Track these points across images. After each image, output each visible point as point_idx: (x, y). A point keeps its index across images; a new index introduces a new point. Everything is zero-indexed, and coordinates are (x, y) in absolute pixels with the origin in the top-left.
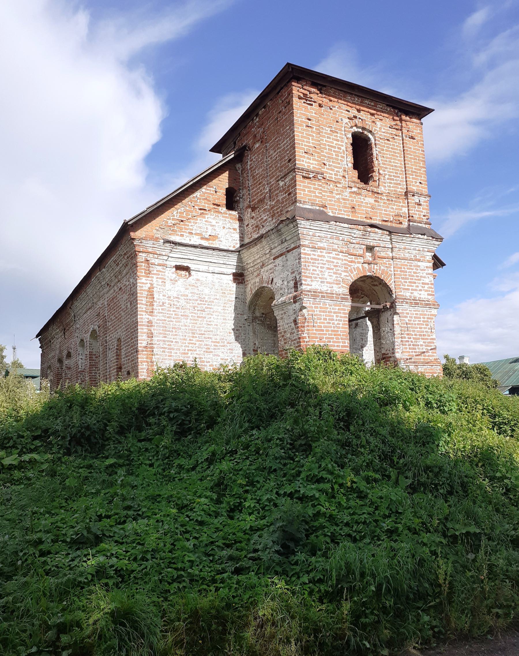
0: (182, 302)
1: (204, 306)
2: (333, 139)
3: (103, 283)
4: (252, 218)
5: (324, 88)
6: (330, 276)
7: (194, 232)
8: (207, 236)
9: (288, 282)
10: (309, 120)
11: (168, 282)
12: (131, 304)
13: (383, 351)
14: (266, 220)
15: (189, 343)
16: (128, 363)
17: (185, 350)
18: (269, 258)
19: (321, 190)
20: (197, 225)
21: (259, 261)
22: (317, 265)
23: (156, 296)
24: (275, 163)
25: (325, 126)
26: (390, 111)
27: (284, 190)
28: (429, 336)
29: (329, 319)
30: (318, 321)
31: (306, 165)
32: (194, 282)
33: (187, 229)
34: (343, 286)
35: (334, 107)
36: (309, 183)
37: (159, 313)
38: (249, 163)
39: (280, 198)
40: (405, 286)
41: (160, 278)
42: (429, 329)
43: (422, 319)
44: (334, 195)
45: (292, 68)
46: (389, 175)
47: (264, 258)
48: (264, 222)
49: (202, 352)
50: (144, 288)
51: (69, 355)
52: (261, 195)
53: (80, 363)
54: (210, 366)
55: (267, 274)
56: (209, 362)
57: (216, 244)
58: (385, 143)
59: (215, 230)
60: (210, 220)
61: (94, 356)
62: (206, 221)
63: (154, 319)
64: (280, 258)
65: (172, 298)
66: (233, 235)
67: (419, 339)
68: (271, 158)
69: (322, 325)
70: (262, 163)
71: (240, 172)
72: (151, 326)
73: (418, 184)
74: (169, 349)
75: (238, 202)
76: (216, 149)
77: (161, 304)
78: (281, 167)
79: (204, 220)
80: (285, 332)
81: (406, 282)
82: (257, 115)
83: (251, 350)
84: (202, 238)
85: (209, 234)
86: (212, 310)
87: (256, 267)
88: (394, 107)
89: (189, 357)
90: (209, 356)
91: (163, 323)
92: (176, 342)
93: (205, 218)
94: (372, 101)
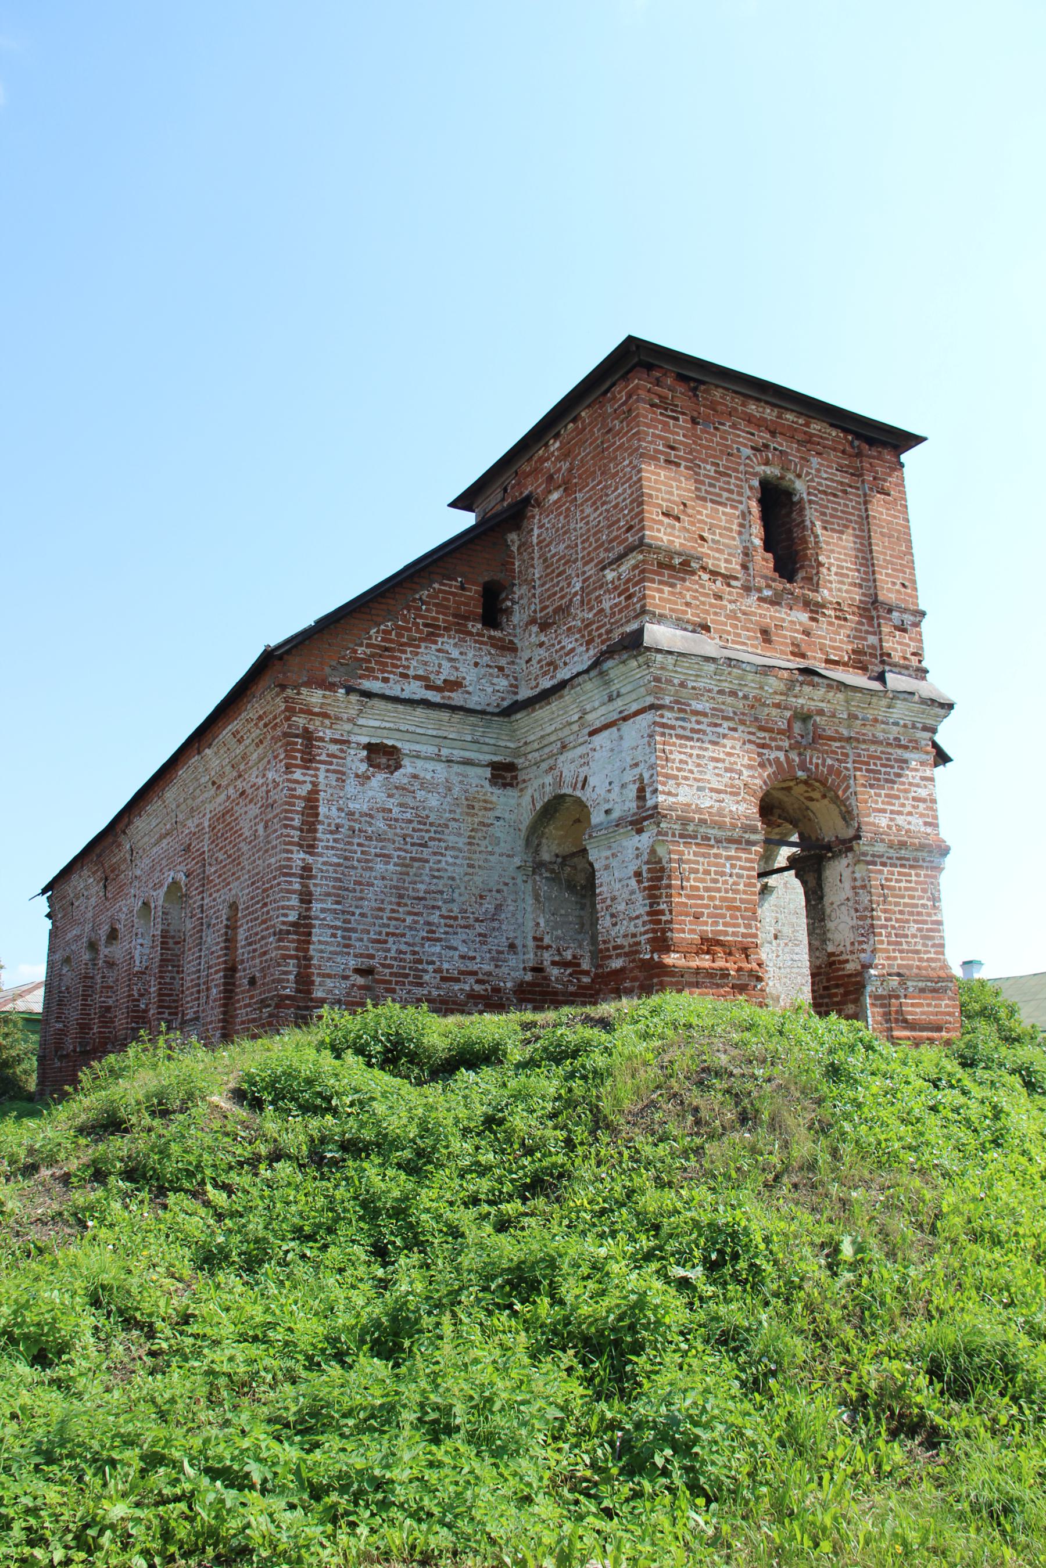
0: (380, 824)
1: (427, 836)
2: (721, 488)
3: (203, 780)
4: (541, 645)
5: (702, 387)
6: (718, 775)
7: (411, 672)
8: (439, 683)
9: (623, 786)
10: (673, 448)
11: (351, 782)
12: (266, 827)
13: (830, 948)
14: (573, 650)
15: (390, 919)
16: (253, 958)
17: (380, 933)
18: (577, 733)
19: (697, 591)
20: (419, 657)
21: (553, 738)
22: (688, 750)
23: (322, 810)
24: (595, 534)
25: (705, 462)
26: (837, 436)
27: (616, 588)
28: (929, 915)
29: (716, 873)
30: (692, 876)
31: (665, 538)
32: (405, 781)
33: (398, 667)
34: (744, 800)
35: (723, 424)
36: (670, 576)
37: (327, 848)
38: (536, 532)
39: (606, 605)
40: (876, 802)
41: (335, 772)
42: (929, 899)
43: (914, 878)
44: (725, 603)
45: (638, 347)
46: (839, 567)
47: (567, 731)
48: (567, 654)
49: (418, 940)
50: (297, 793)
51: (113, 935)
52: (562, 597)
53: (137, 955)
54: (435, 971)
55: (572, 767)
56: (433, 963)
57: (457, 698)
58: (829, 501)
59: (457, 669)
60: (446, 647)
61: (170, 941)
62: (439, 650)
63: (317, 863)
64: (605, 734)
65: (357, 816)
66: (495, 680)
67: (907, 921)
68: (587, 523)
69: (701, 885)
70: (565, 533)
71: (514, 549)
72: (310, 877)
73: (898, 587)
74: (345, 930)
75: (509, 612)
76: (463, 502)
77: (333, 828)
78: (611, 541)
79: (434, 647)
80: (613, 899)
81: (879, 795)
82: (557, 436)
83: (530, 938)
84: (428, 687)
85: (442, 677)
86: (443, 844)
87: (547, 750)
88: (845, 431)
89: (389, 950)
90: (433, 949)
91: (336, 872)
92: (362, 915)
93: (436, 643)
94: (800, 414)
